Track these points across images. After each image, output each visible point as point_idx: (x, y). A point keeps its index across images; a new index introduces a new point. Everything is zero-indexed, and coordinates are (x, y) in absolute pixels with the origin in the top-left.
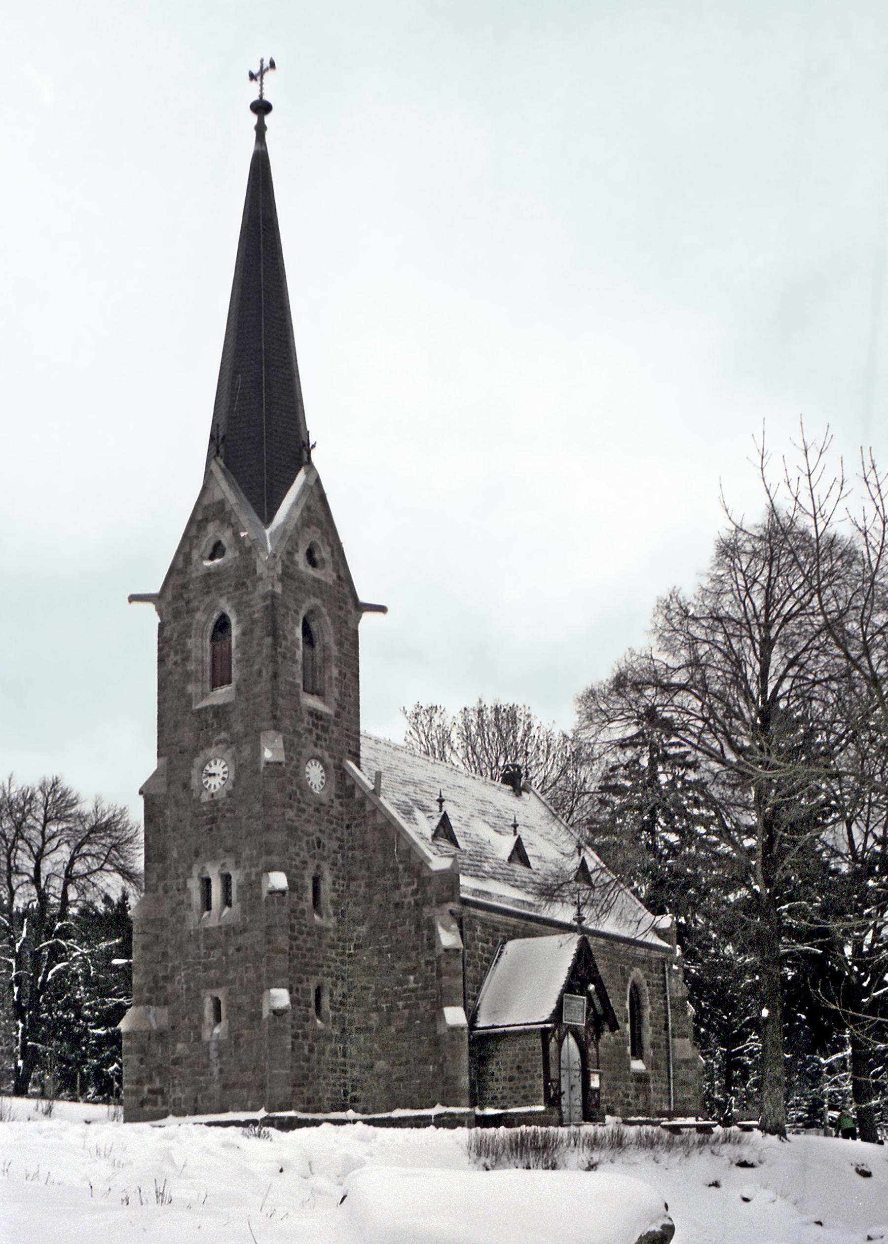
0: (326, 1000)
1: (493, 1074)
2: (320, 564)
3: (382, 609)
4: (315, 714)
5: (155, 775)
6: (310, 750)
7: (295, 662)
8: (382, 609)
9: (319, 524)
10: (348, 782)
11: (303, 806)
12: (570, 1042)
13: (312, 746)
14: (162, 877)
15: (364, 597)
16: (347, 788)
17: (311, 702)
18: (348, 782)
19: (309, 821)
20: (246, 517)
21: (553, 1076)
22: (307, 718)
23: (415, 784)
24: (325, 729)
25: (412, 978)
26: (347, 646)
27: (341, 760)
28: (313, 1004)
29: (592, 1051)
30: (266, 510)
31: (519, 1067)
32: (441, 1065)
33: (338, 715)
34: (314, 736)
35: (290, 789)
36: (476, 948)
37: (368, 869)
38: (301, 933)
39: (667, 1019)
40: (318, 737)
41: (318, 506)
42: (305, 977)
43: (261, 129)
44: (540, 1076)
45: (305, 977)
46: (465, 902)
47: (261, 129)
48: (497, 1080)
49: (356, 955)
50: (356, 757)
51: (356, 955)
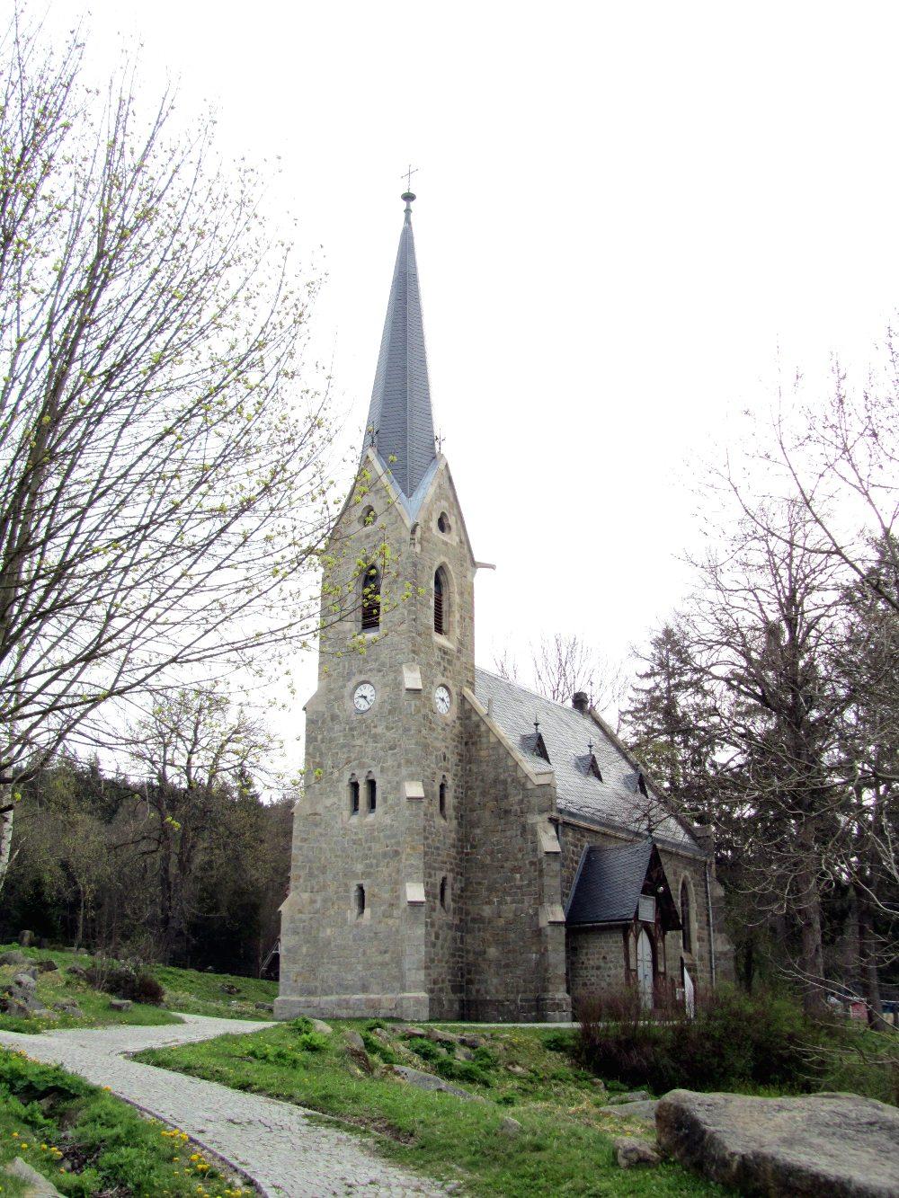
0: (448, 893)
1: (583, 963)
2: (447, 530)
3: (492, 567)
4: (444, 651)
5: (316, 696)
6: (440, 679)
7: (429, 608)
8: (492, 567)
9: (447, 499)
10: (467, 707)
11: (433, 725)
12: (644, 938)
13: (440, 675)
14: (318, 780)
15: (477, 559)
16: (465, 711)
17: (440, 639)
18: (467, 707)
19: (437, 739)
20: (394, 492)
21: (632, 967)
22: (437, 653)
23: (102, 415)
24: (450, 662)
25: (518, 876)
26: (466, 596)
27: (461, 688)
28: (439, 897)
29: (660, 944)
30: (408, 487)
31: (604, 958)
32: (543, 955)
33: (459, 651)
34: (442, 668)
35: (423, 711)
36: (568, 851)
37: (482, 780)
38: (431, 834)
39: (708, 915)
40: (445, 669)
41: (446, 485)
42: (433, 872)
43: (408, 211)
44: (137, 969)
45: (433, 872)
46: (560, 811)
47: (408, 211)
48: (586, 968)
49: (472, 854)
50: (471, 684)
51: (472, 854)
